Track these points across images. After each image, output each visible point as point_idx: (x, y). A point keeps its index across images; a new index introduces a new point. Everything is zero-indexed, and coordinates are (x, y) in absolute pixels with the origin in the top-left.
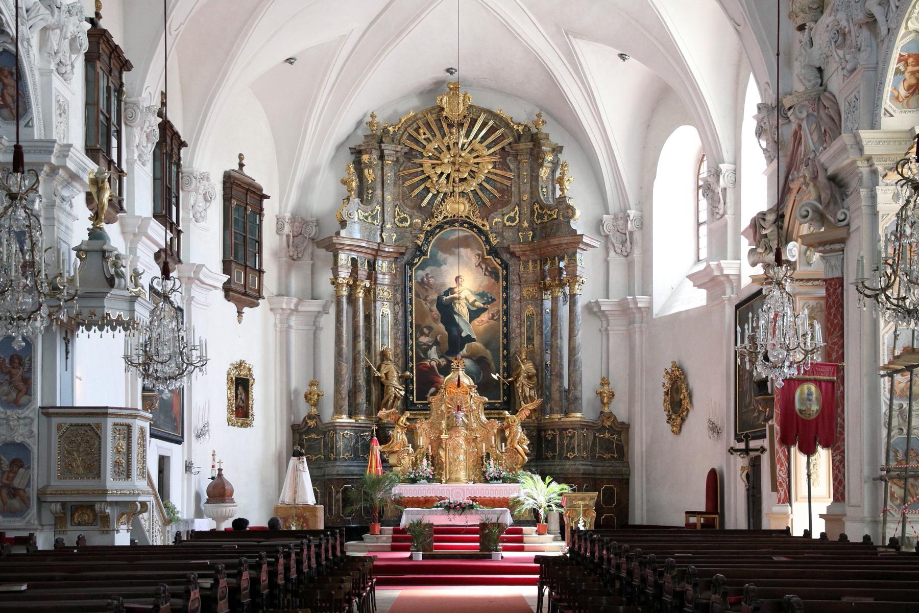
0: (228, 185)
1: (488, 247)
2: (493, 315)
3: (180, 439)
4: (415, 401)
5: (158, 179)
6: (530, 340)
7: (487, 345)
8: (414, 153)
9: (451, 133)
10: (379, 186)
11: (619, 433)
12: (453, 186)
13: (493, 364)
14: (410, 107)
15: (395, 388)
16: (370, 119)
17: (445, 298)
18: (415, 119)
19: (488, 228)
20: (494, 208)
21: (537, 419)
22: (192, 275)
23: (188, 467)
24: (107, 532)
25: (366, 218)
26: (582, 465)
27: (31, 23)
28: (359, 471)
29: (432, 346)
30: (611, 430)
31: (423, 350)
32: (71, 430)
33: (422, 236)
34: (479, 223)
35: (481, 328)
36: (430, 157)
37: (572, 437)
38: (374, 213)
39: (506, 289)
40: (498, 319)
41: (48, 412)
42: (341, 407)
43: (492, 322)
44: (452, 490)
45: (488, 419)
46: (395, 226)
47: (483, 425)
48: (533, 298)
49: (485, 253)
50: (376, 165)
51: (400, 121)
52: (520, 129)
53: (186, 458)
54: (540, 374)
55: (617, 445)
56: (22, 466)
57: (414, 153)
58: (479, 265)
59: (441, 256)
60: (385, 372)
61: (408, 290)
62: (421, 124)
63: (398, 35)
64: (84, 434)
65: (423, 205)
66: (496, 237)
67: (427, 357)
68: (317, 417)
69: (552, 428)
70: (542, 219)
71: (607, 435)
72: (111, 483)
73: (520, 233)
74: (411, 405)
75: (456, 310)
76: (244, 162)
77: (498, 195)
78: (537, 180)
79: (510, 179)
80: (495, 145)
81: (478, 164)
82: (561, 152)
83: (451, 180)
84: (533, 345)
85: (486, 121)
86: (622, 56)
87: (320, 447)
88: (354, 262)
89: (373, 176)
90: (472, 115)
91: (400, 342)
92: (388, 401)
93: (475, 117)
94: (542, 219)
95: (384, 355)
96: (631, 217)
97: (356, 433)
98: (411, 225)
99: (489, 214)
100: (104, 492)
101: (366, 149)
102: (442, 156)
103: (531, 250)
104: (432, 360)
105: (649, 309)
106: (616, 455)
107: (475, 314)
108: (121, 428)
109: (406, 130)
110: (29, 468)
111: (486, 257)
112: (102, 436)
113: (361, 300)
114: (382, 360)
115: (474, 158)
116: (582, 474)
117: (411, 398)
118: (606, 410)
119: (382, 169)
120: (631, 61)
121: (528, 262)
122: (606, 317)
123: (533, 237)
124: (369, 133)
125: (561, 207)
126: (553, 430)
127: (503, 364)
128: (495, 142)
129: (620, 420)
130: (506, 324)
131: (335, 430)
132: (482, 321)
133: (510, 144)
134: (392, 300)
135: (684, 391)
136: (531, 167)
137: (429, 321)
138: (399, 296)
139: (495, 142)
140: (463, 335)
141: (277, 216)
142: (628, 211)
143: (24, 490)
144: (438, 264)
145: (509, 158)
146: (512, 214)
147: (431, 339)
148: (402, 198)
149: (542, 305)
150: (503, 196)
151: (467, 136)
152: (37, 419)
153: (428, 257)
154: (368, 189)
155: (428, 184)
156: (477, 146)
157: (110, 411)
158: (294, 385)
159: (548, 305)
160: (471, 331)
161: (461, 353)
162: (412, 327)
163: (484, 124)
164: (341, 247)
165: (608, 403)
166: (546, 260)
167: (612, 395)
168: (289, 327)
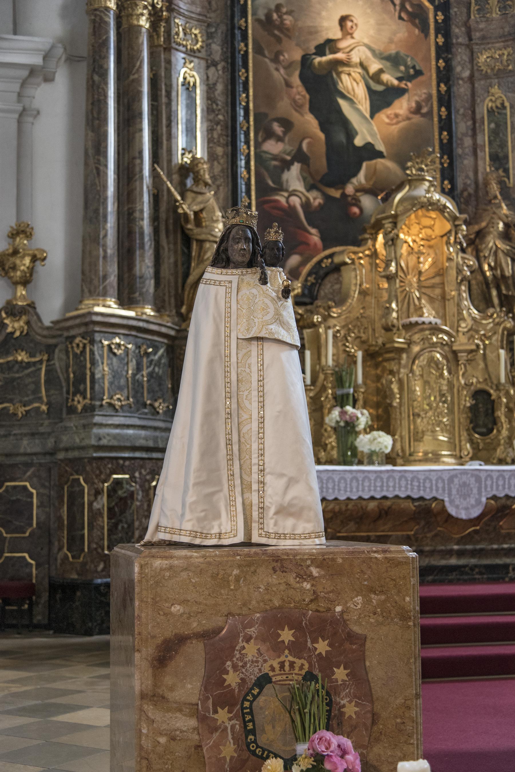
17: (318, 60)
28: (146, 439)
35: (395, 129)
40: (430, 113)
43: (417, 119)
67: (280, 188)
75: (340, 87)
87: (37, 383)
91: (220, 151)
97: (139, 347)
104: (293, 193)
132: (397, 116)
134: (203, 54)
138: (216, 48)
140: (358, 142)
147: (289, 148)
160: (373, 135)
161: (354, 180)
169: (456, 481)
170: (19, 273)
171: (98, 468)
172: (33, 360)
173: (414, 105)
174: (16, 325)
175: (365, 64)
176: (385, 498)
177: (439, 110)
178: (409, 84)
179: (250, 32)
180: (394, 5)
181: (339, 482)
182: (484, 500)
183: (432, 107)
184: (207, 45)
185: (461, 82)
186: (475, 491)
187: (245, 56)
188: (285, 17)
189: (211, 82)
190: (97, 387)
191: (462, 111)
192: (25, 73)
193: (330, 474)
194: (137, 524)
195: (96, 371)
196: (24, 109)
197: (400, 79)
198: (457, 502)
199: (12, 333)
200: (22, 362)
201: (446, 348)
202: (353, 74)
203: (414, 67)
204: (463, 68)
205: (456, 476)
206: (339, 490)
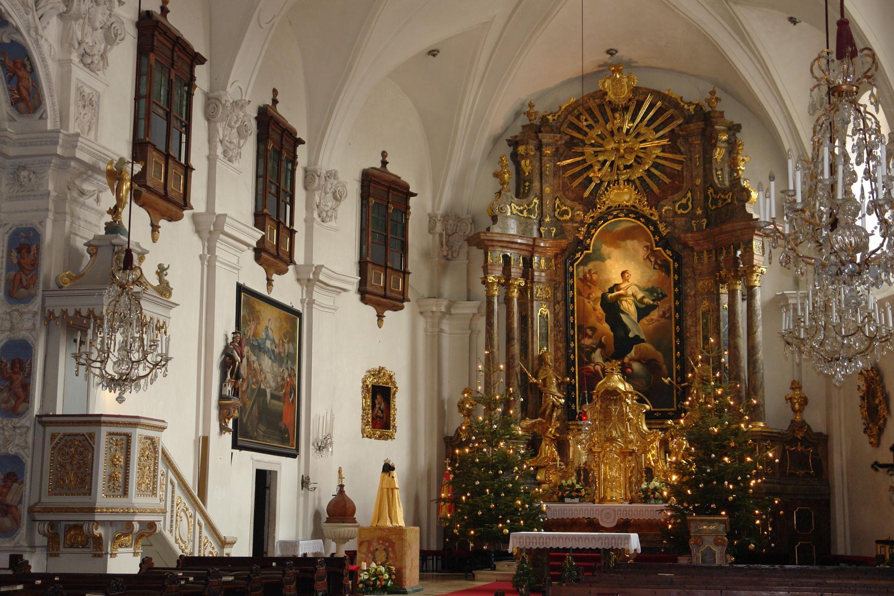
0: (366, 183)
2: (664, 313)
3: (295, 452)
5: (260, 177)
7: (658, 347)
8: (575, 141)
9: (615, 119)
12: (618, 174)
13: (664, 367)
14: (570, 96)
15: (554, 396)
16: (528, 109)
17: (610, 295)
18: (576, 105)
22: (311, 277)
23: (305, 483)
24: (100, 556)
27: (40, 12)
30: (804, 441)
31: (586, 354)
32: (66, 441)
34: (647, 210)
36: (592, 145)
38: (531, 207)
41: (46, 420)
43: (663, 320)
45: (650, 429)
46: (555, 220)
47: (643, 436)
48: (709, 293)
51: (560, 109)
52: (692, 108)
53: (302, 473)
56: (16, 481)
57: (575, 141)
58: (648, 257)
59: (605, 249)
61: (569, 287)
64: (78, 445)
67: (590, 361)
70: (716, 204)
72: (102, 499)
73: (693, 221)
75: (622, 307)
76: (387, 159)
77: (667, 181)
78: (710, 162)
80: (664, 128)
81: (645, 148)
82: (739, 131)
83: (615, 168)
86: (793, 21)
88: (506, 259)
90: (638, 95)
91: (561, 345)
92: (545, 410)
93: (641, 99)
94: (716, 204)
99: (658, 202)
100: (92, 510)
101: (522, 140)
102: (605, 143)
103: (704, 239)
104: (597, 364)
107: (643, 311)
108: (119, 438)
109: (566, 117)
110: (22, 482)
111: (655, 249)
112: (95, 447)
113: (515, 300)
114: (540, 365)
115: (641, 142)
117: (573, 406)
119: (541, 160)
120: (803, 25)
124: (528, 122)
125: (735, 190)
127: (676, 367)
128: (664, 125)
130: (679, 322)
132: (652, 320)
133: (680, 125)
134: (552, 298)
135: (879, 394)
136: (703, 149)
137: (592, 321)
138: (559, 295)
140: (631, 335)
141: (429, 215)
143: (16, 507)
144: (602, 259)
145: (679, 141)
146: (684, 201)
147: (595, 341)
151: (633, 120)
152: (32, 428)
154: (525, 182)
156: (643, 130)
157: (103, 419)
158: (446, 394)
159: (725, 299)
160: (639, 331)
161: (629, 355)
164: (490, 243)
165: (801, 411)
166: (721, 249)
168: (441, 331)
173: (661, 313)
180: (651, 262)
189: (557, 311)
191: (690, 313)
192: (472, 316)
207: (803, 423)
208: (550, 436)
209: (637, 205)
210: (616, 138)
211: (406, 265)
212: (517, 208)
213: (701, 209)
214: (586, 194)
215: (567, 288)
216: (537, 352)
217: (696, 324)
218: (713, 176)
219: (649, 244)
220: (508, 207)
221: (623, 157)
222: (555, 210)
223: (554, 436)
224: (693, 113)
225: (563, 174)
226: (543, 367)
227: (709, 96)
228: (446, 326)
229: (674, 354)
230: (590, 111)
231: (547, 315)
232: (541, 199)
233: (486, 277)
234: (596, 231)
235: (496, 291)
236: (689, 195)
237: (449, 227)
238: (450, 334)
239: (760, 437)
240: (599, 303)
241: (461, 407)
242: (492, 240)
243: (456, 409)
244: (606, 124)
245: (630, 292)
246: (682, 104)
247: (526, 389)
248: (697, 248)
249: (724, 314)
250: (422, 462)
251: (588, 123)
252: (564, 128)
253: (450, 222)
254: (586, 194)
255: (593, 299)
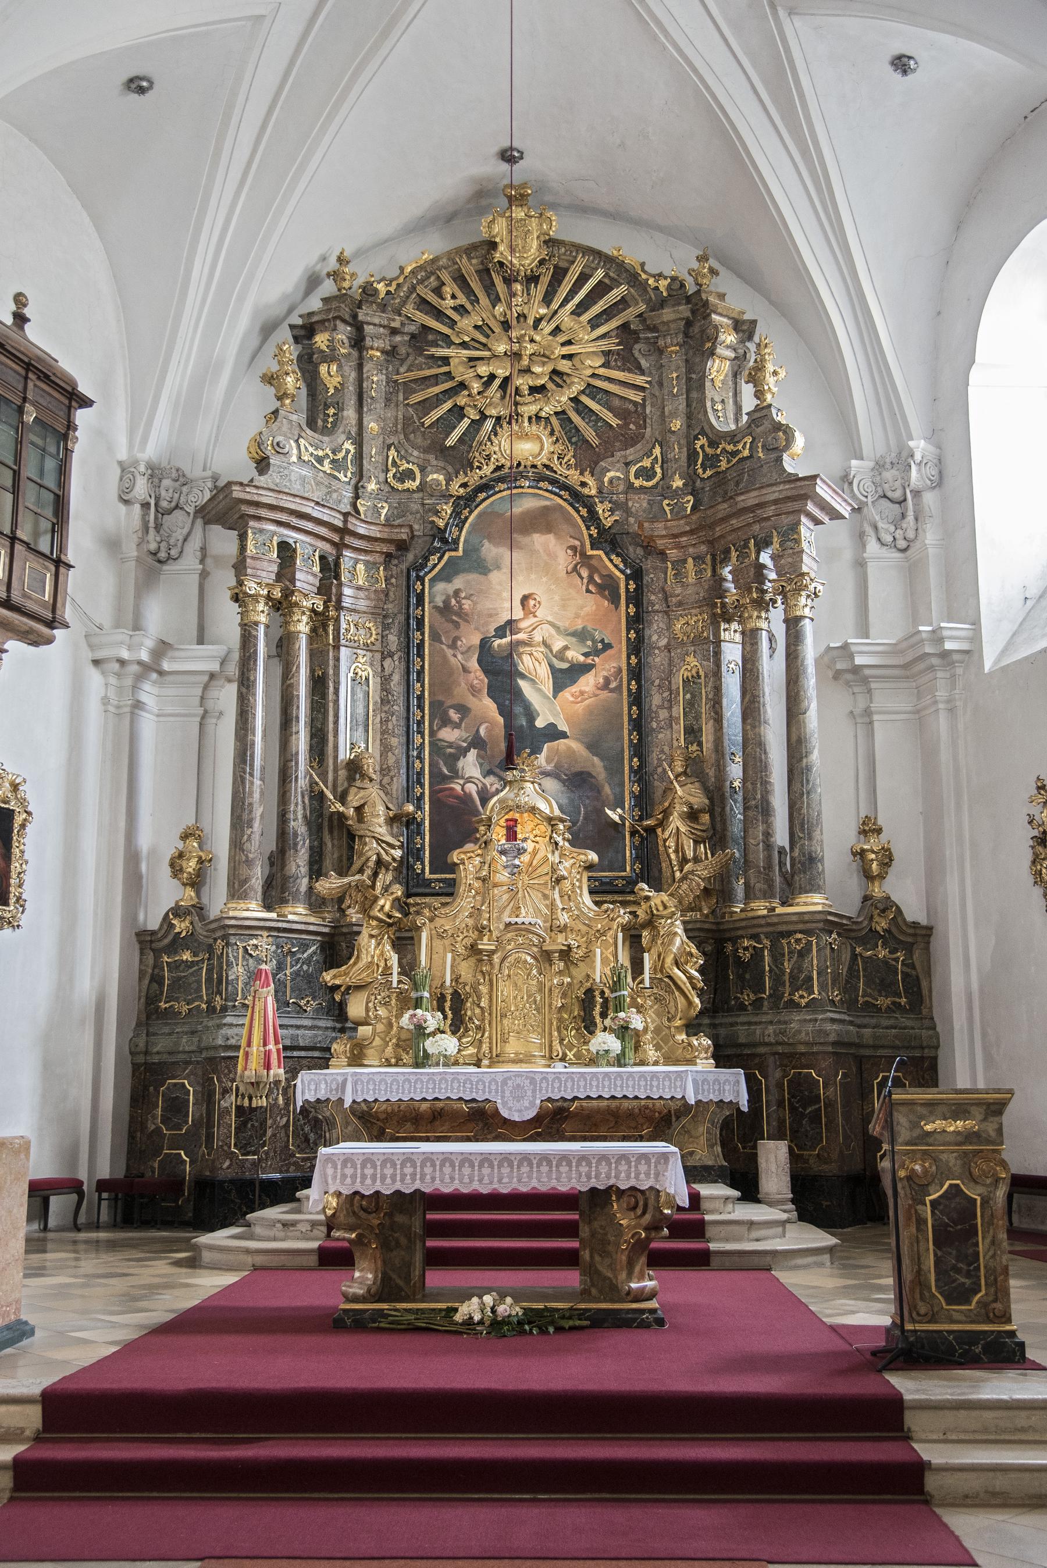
1: (594, 532)
2: (607, 681)
4: (427, 875)
6: (693, 733)
7: (593, 747)
8: (430, 337)
9: (512, 295)
10: (351, 402)
11: (909, 948)
13: (607, 789)
17: (497, 642)
19: (594, 492)
20: (607, 449)
21: (713, 912)
25: (320, 460)
26: (833, 1021)
29: (466, 750)
30: (889, 938)
33: (448, 509)
34: (573, 477)
35: (580, 708)
37: (804, 953)
39: (636, 622)
40: (619, 688)
42: (246, 881)
43: (605, 695)
44: (504, 1082)
46: (387, 489)
48: (698, 641)
49: (588, 546)
50: (347, 356)
52: (663, 284)
54: (718, 810)
55: (905, 975)
58: (575, 569)
59: (490, 550)
60: (356, 804)
61: (413, 624)
62: (445, 277)
63: (385, 34)
65: (450, 442)
66: (611, 510)
67: (455, 774)
68: (199, 909)
69: (751, 931)
71: (882, 953)
74: (418, 886)
76: (27, 312)
77: (614, 422)
78: (701, 387)
79: (642, 389)
80: (607, 321)
83: (511, 390)
84: (700, 744)
85: (587, 271)
87: (199, 982)
88: (286, 550)
89: (339, 379)
93: (563, 264)
95: (354, 768)
96: (918, 457)
98: (421, 489)
99: (596, 463)
104: (469, 780)
105: (972, 654)
106: (903, 1001)
109: (413, 288)
111: (590, 553)
114: (351, 779)
115: (563, 344)
116: (835, 1044)
117: (418, 866)
118: (877, 891)
119: (360, 367)
121: (685, 561)
122: (865, 681)
123: (694, 508)
125: (759, 430)
126: (755, 937)
128: (607, 314)
129: (909, 918)
131: (225, 937)
132: (582, 693)
133: (640, 315)
134: (378, 646)
136: (687, 361)
138: (393, 639)
139: (607, 314)
140: (540, 723)
142: (911, 444)
145: (637, 346)
146: (647, 463)
147: (465, 735)
148: (403, 428)
149: (718, 654)
150: (626, 425)
151: (547, 300)
153: (460, 553)
154: (327, 406)
155: (462, 400)
158: (145, 841)
159: (732, 652)
160: (556, 715)
162: (421, 707)
163: (583, 278)
164: (251, 511)
165: (881, 877)
166: (727, 551)
167: (887, 858)
168: (138, 705)
169: (510, 1083)
170: (185, 875)
171: (227, 1067)
172: (196, 959)
173: (601, 680)
174: (183, 925)
175: (548, 642)
176: (436, 1099)
177: (629, 684)
178: (596, 659)
179: (426, 620)
180: (582, 578)
181: (391, 1084)
182: (538, 1102)
183: (621, 681)
184: (382, 637)
185: (657, 651)
186: (529, 1093)
187: (421, 646)
188: (464, 601)
189: (386, 673)
190: (230, 988)
191: (657, 682)
192: (206, 678)
193: (383, 1076)
194: (269, 1122)
195: (230, 973)
196: (206, 712)
197: (585, 655)
198: (510, 1104)
199: (180, 933)
200: (187, 961)
201: (535, 949)
202: (535, 654)
203: (602, 641)
204: (660, 636)
205: (510, 1078)
206: (391, 1092)
207: (887, 905)
208: (380, 915)
209: (555, 464)
210: (514, 334)
211: (62, 549)
212: (311, 449)
213: (681, 478)
214: (451, 440)
215: (410, 625)
216: (344, 754)
217: (670, 704)
218: (706, 412)
219: (577, 543)
220: (294, 444)
221: (527, 371)
222: (388, 470)
223: (390, 917)
224: (665, 294)
225: (406, 399)
226: (358, 783)
227: (695, 265)
228: (149, 693)
229: (626, 762)
230: (461, 280)
231: (367, 679)
232: (359, 444)
233: (240, 583)
234: (471, 512)
235: (261, 613)
236: (657, 451)
237: (163, 493)
238: (158, 716)
239: (821, 925)
240: (476, 656)
241: (176, 866)
242: (257, 504)
243: (167, 870)
244: (494, 307)
245: (538, 637)
246: (644, 276)
247: (320, 828)
248: (673, 553)
249: (732, 685)
250: (85, 987)
251: (458, 302)
252: (410, 309)
253: (166, 482)
254: (451, 440)
255: (464, 649)
